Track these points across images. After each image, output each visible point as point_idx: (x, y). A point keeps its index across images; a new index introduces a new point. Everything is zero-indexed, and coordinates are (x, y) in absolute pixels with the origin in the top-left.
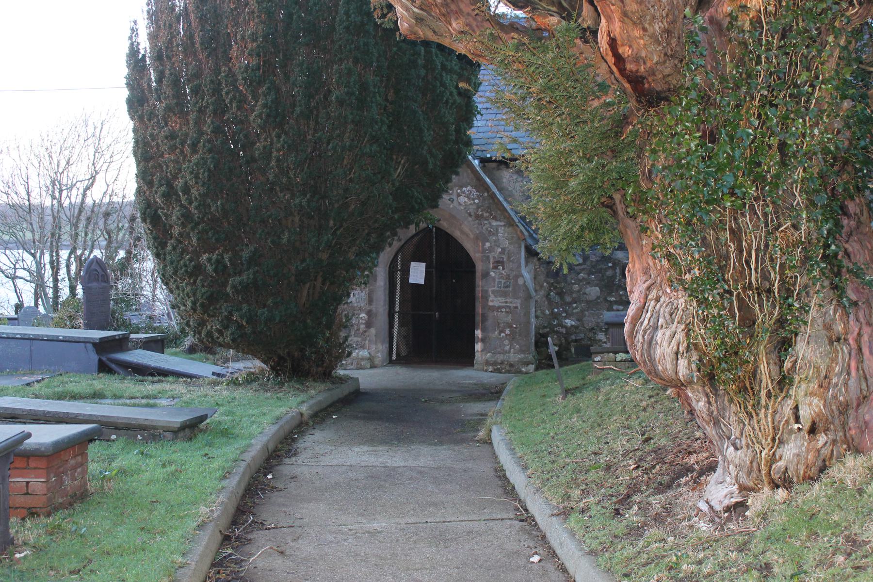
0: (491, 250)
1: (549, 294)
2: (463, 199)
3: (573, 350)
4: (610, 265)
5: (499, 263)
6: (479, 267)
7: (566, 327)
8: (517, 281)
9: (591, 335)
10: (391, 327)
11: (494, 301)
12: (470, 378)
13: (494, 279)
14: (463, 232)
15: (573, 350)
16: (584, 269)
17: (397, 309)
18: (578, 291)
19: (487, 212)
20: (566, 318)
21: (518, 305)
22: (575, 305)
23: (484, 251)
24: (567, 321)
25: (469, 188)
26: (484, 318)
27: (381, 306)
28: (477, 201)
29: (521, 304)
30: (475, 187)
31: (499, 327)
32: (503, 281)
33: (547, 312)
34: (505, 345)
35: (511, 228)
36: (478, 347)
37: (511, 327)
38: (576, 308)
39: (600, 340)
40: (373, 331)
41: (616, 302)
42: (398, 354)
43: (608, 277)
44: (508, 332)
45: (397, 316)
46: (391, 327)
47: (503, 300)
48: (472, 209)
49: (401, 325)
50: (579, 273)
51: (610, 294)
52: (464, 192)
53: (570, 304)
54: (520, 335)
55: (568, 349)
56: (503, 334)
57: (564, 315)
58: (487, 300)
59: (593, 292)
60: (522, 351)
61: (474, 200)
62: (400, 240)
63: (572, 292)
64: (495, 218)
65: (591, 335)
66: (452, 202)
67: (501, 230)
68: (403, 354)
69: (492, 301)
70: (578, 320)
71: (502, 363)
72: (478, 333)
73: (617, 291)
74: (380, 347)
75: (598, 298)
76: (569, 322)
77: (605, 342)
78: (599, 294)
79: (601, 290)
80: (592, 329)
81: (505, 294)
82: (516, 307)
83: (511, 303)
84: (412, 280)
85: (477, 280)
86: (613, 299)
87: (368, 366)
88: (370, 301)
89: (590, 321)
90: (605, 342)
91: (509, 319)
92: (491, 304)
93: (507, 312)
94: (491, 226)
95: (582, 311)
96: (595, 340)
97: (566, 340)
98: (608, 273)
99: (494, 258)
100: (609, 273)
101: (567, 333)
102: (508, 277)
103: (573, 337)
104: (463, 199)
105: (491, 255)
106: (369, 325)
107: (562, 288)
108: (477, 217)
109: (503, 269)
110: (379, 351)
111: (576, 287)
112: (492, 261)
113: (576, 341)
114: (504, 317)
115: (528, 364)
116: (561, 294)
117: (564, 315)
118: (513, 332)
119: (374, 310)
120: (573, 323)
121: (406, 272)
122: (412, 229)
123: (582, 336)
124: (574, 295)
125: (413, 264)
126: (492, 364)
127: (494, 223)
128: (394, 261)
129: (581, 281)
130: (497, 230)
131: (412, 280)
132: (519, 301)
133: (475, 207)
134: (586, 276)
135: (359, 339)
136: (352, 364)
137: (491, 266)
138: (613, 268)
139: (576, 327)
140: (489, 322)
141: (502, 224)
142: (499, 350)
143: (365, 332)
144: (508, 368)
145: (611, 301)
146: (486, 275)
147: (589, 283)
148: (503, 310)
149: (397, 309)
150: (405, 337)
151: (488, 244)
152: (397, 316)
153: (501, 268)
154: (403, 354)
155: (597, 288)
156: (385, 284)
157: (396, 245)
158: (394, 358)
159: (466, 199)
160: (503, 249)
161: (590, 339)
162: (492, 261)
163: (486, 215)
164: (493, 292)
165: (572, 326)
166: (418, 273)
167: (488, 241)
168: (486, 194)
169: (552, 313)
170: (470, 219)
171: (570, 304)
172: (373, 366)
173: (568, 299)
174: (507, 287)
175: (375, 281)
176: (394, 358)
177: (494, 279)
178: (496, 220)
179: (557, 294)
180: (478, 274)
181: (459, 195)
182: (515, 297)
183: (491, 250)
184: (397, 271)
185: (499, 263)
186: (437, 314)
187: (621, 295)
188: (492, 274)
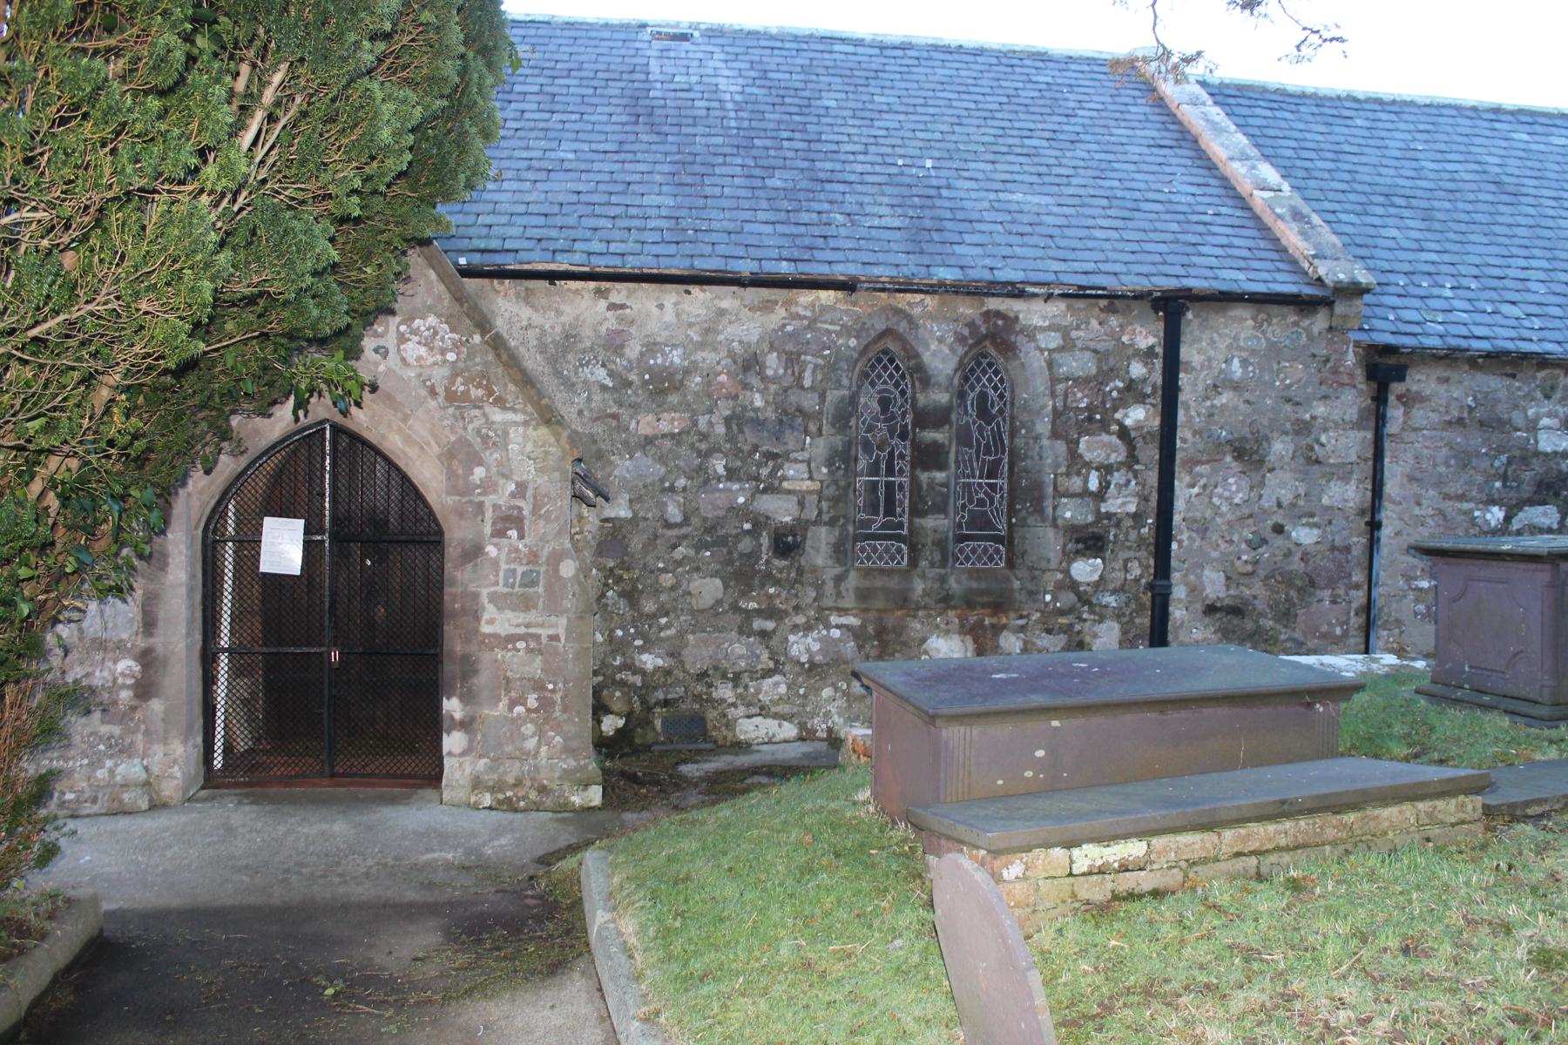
0: (488, 486)
1: (603, 595)
2: (413, 350)
3: (658, 723)
4: (747, 526)
5: (509, 521)
6: (456, 533)
7: (643, 673)
8: (556, 570)
9: (699, 688)
10: (209, 680)
11: (496, 621)
12: (444, 838)
13: (495, 563)
14: (408, 440)
15: (658, 723)
16: (685, 537)
17: (225, 642)
18: (673, 588)
19: (479, 386)
20: (642, 650)
21: (561, 632)
22: (663, 621)
23: (467, 490)
24: (645, 657)
25: (432, 320)
26: (469, 667)
27: (178, 637)
28: (451, 357)
29: (568, 630)
30: (449, 320)
31: (508, 691)
32: (520, 570)
33: (599, 638)
34: (524, 738)
35: (543, 431)
36: (452, 742)
37: (539, 686)
38: (668, 626)
39: (723, 700)
40: (156, 705)
41: (759, 613)
42: (228, 749)
43: (742, 555)
44: (532, 701)
45: (224, 659)
46: (209, 680)
47: (521, 617)
48: (439, 375)
49: (236, 672)
50: (674, 547)
51: (744, 594)
52: (416, 332)
53: (654, 616)
54: (565, 709)
55: (648, 723)
56: (519, 709)
57: (638, 642)
58: (478, 619)
59: (708, 589)
60: (568, 750)
61: (443, 352)
62: (238, 452)
63: (657, 591)
64: (500, 402)
65: (699, 688)
66: (385, 355)
67: (515, 434)
68: (241, 746)
69: (491, 622)
70: (672, 655)
71: (518, 783)
72: (452, 706)
73: (762, 586)
74: (178, 749)
75: (719, 602)
76: (649, 661)
77: (734, 705)
78: (720, 595)
79: (726, 587)
80: (702, 676)
81: (526, 604)
82: (554, 638)
83: (542, 626)
84: (266, 566)
85: (448, 566)
86: (753, 605)
87: (144, 805)
88: (149, 624)
89: (698, 655)
90: (734, 705)
91: (536, 668)
92: (486, 629)
93: (529, 651)
94: (490, 424)
95: (681, 634)
96: (710, 700)
97: (643, 702)
98: (741, 546)
99: (496, 507)
100: (746, 545)
101: (645, 686)
102: (533, 557)
103: (660, 695)
104: (413, 350)
105: (489, 500)
106: (144, 689)
107: (634, 581)
108: (451, 397)
109: (521, 537)
110: (172, 759)
111: (667, 580)
112: (489, 514)
113: (666, 703)
114: (519, 663)
115: (586, 786)
116: (631, 596)
117: (638, 642)
118: (545, 704)
119: (160, 650)
120: (660, 662)
121: (250, 543)
122: (283, 419)
123: (680, 690)
124: (663, 597)
125: (269, 522)
126: (492, 790)
127: (498, 416)
128: (218, 512)
129: (679, 563)
130: (506, 433)
131: (266, 566)
132: (563, 621)
133: (445, 371)
134: (692, 552)
135: (116, 730)
136: (94, 800)
137: (488, 529)
138: (754, 533)
139: (668, 672)
140: (483, 679)
141: (520, 417)
142: (509, 749)
143: (134, 709)
144: (533, 795)
145: (746, 611)
146: (474, 553)
147: (698, 569)
148: (521, 645)
149: (225, 642)
150: (245, 702)
151: (479, 473)
152: (224, 659)
153: (513, 533)
154: (241, 746)
155: (718, 582)
156: (192, 576)
157: (228, 465)
158: (218, 762)
159: (423, 351)
160: (521, 489)
161: (698, 698)
162: (489, 514)
163: (477, 393)
164: (494, 598)
165: (657, 669)
166: (283, 546)
167: (480, 463)
168: (477, 339)
169: (611, 639)
170: (432, 404)
171: (654, 616)
172: (156, 806)
173: (649, 606)
174: (533, 583)
175: (163, 567)
176: (218, 762)
177: (495, 563)
178: (504, 408)
179: (621, 594)
180: (452, 552)
181: (402, 339)
182: (553, 608)
183: (488, 486)
184: (226, 540)
185: (509, 521)
186: (335, 656)
187: (770, 597)
188: (491, 550)
